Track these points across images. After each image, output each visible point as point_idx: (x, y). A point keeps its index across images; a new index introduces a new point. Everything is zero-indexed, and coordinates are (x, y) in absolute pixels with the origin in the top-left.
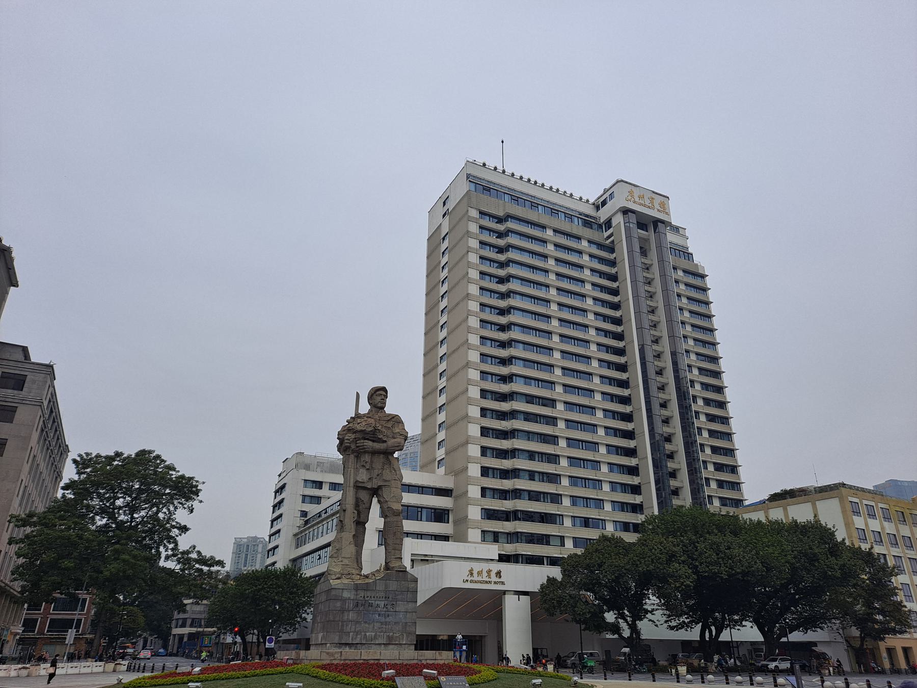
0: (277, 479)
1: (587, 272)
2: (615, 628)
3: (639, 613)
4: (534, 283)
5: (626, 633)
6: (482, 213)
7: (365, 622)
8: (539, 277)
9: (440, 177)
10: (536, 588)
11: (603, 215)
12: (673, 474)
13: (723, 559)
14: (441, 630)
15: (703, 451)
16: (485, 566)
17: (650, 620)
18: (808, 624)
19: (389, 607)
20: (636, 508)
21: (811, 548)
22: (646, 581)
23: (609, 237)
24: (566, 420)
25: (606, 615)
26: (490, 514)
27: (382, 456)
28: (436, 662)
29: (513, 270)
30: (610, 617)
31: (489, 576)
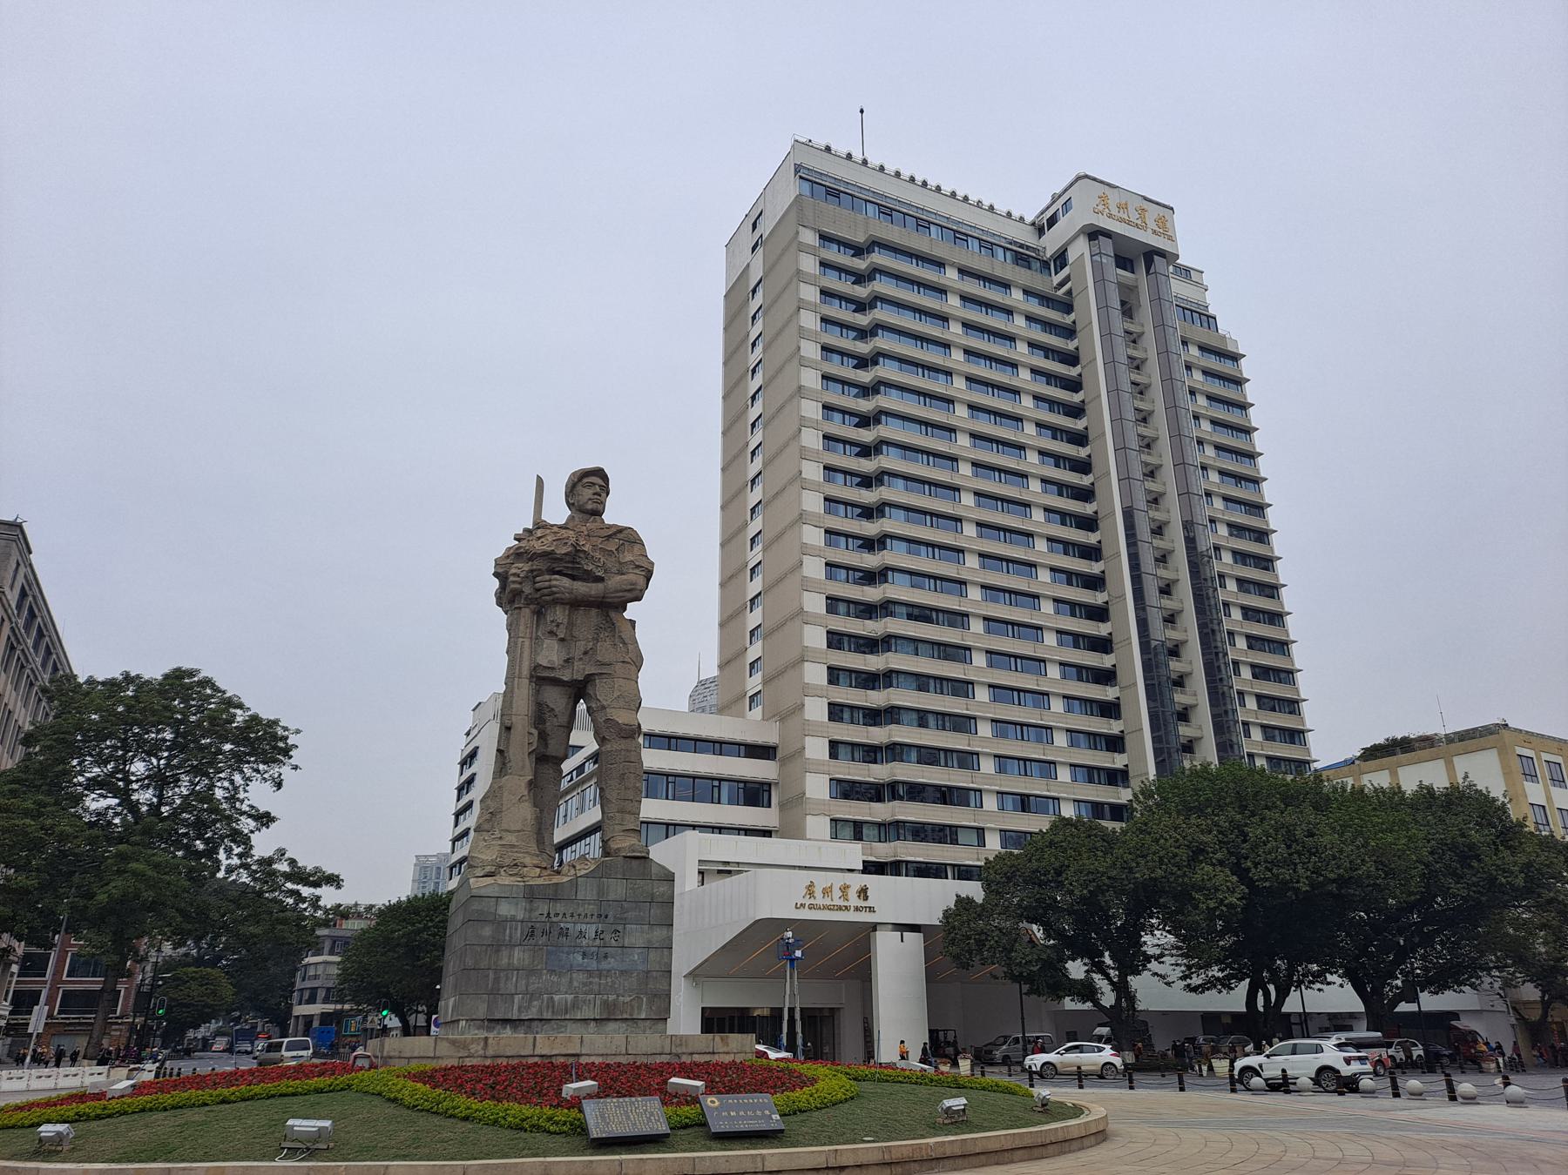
1: (1022, 348)
2: (1086, 991)
3: (1133, 960)
4: (923, 367)
5: (1108, 998)
6: (825, 238)
7: (552, 972)
10: (934, 918)
11: (1050, 243)
12: (1184, 715)
13: (1299, 854)
14: (758, 1001)
15: (1237, 673)
16: (838, 880)
17: (1155, 974)
18: (1440, 981)
19: (607, 936)
20: (1116, 777)
21: (1463, 835)
22: (1147, 900)
23: (1062, 284)
24: (986, 619)
25: (1069, 965)
26: (847, 790)
27: (594, 611)
29: (883, 342)
30: (1076, 969)
31: (845, 896)
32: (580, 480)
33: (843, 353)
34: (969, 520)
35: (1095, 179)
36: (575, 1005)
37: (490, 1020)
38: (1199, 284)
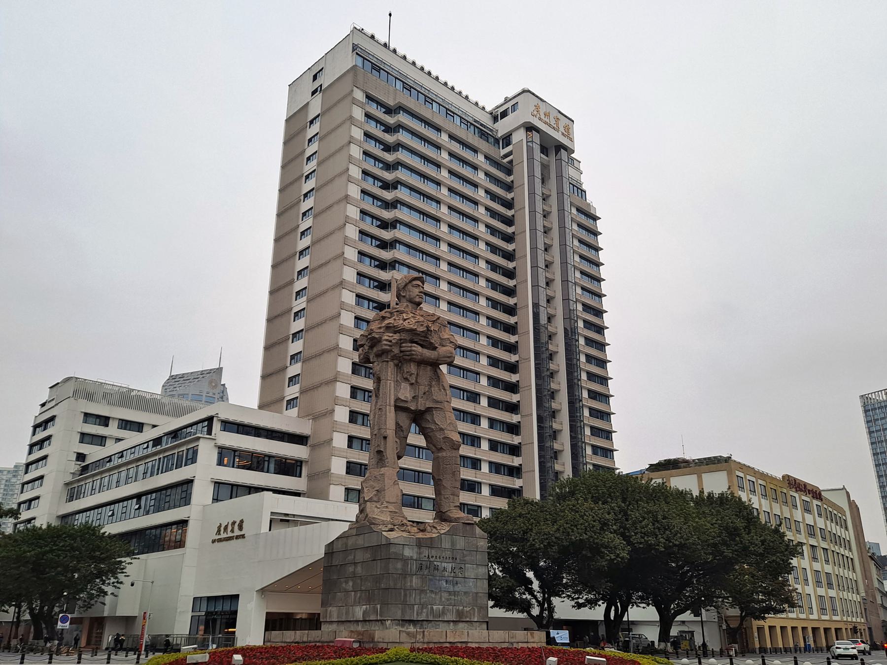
0: (38, 410)
4: (424, 195)
6: (369, 97)
8: (429, 188)
9: (314, 41)
11: (502, 128)
13: (659, 529)
19: (457, 571)
23: (506, 156)
27: (429, 368)
28: (530, 646)
29: (402, 174)
31: (232, 531)
32: (410, 282)
33: (375, 178)
34: (444, 299)
35: (533, 94)
36: (443, 613)
37: (403, 620)
38: (578, 169)
